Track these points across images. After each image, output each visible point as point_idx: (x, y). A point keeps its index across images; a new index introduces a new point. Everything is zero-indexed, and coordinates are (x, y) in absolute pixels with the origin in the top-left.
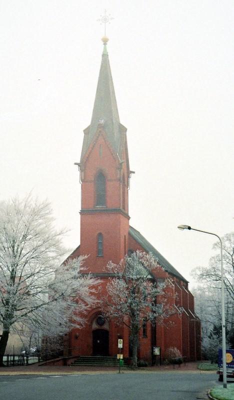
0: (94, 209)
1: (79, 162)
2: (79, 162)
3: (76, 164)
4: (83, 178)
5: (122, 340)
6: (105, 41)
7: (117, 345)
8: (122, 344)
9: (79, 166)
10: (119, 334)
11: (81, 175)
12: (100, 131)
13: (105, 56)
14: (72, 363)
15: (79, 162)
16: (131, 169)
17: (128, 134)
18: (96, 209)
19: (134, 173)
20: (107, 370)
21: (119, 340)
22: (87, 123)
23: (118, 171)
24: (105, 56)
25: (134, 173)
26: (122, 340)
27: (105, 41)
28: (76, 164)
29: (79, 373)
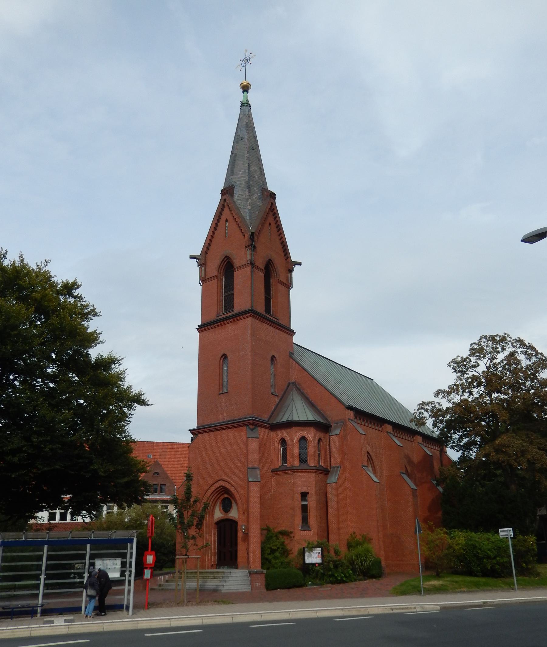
3: (192, 257)
4: (203, 276)
6: (246, 88)
13: (245, 105)
24: (245, 105)
27: (246, 88)
28: (192, 257)
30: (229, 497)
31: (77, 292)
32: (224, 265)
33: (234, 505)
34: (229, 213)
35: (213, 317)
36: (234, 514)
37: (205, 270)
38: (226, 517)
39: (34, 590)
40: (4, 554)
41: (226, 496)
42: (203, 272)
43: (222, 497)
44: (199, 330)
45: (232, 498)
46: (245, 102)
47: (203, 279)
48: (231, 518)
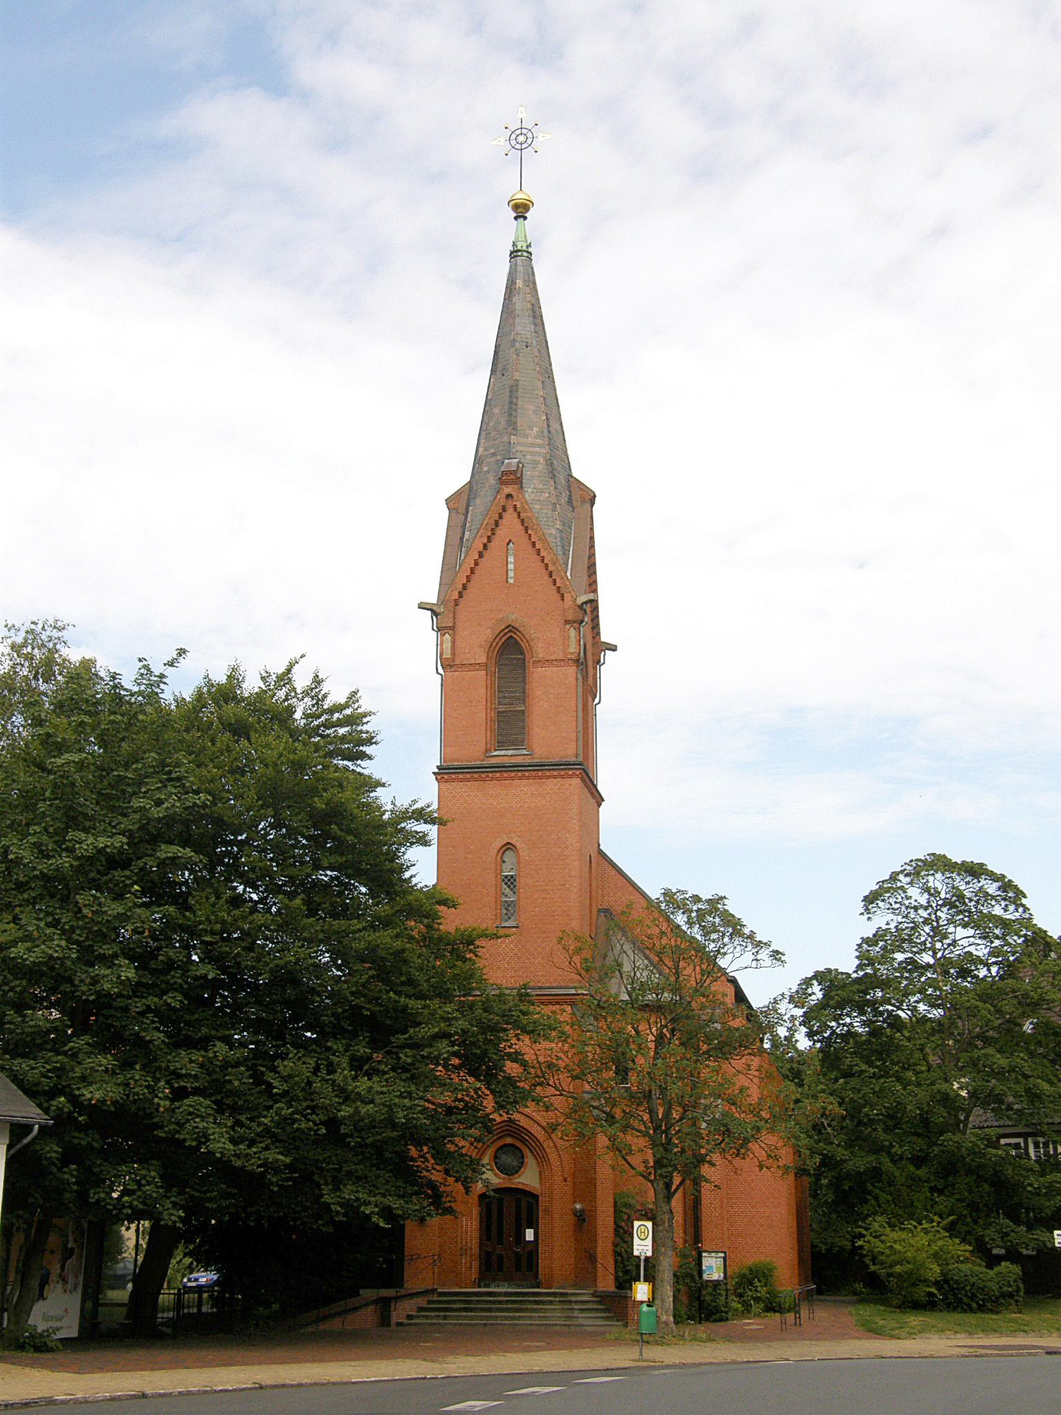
0: (487, 762)
1: (435, 601)
2: (433, 598)
3: (422, 606)
4: (448, 655)
5: (649, 1224)
6: (521, 210)
7: (630, 1245)
8: (649, 1241)
9: (434, 613)
10: (578, 1206)
11: (440, 644)
12: (509, 496)
13: (520, 255)
14: (409, 1317)
15: (433, 598)
16: (605, 637)
17: (600, 511)
18: (493, 761)
19: (613, 648)
20: (322, 1361)
21: (636, 1224)
22: (461, 476)
23: (573, 633)
24: (520, 255)
25: (613, 648)
26: (649, 1224)
27: (521, 210)
28: (422, 606)
29: (963, 1340)
30: (518, 1144)
31: (857, 954)
32: (504, 639)
33: (530, 1160)
34: (517, 522)
35: (474, 749)
36: (528, 1178)
37: (453, 642)
38: (507, 1185)
39: (844, 1336)
40: (642, 1279)
41: (509, 1140)
42: (448, 645)
43: (500, 1143)
44: (439, 777)
45: (523, 1141)
46: (524, 248)
47: (448, 664)
48: (520, 1186)
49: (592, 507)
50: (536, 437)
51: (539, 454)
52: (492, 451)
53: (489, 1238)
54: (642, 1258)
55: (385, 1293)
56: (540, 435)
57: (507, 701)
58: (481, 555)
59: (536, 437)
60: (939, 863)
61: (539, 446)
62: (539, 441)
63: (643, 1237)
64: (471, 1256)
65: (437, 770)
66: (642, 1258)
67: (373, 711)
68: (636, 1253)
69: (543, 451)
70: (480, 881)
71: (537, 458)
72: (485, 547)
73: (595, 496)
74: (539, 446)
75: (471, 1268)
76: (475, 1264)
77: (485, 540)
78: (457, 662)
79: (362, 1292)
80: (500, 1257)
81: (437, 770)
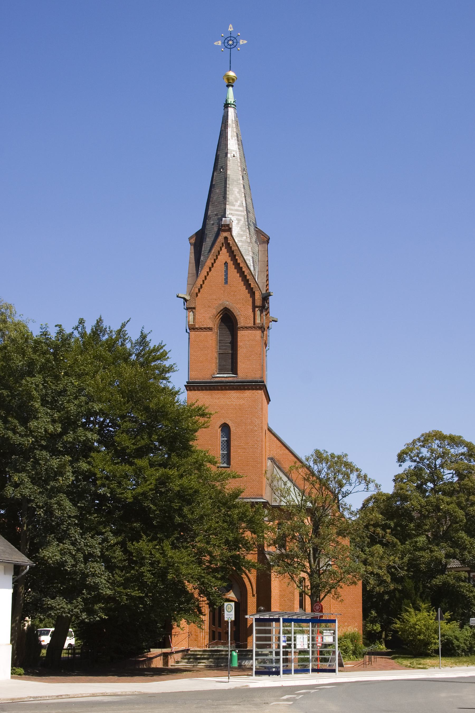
8: (233, 613)
42: (191, 317)
49: (268, 244)
50: (239, 206)
51: (241, 215)
52: (215, 213)
53: (214, 624)
54: (229, 621)
55: (165, 650)
56: (241, 205)
57: (224, 347)
58: (210, 269)
59: (239, 206)
60: (440, 436)
61: (241, 211)
62: (241, 209)
63: (229, 611)
64: (205, 633)
65: (186, 384)
66: (229, 621)
67: (98, 318)
68: (226, 619)
69: (243, 214)
70: (210, 442)
71: (239, 218)
72: (213, 264)
73: (269, 239)
74: (241, 211)
75: (205, 638)
76: (207, 637)
77: (213, 261)
78: (197, 326)
79: (151, 650)
80: (220, 633)
81: (186, 384)
